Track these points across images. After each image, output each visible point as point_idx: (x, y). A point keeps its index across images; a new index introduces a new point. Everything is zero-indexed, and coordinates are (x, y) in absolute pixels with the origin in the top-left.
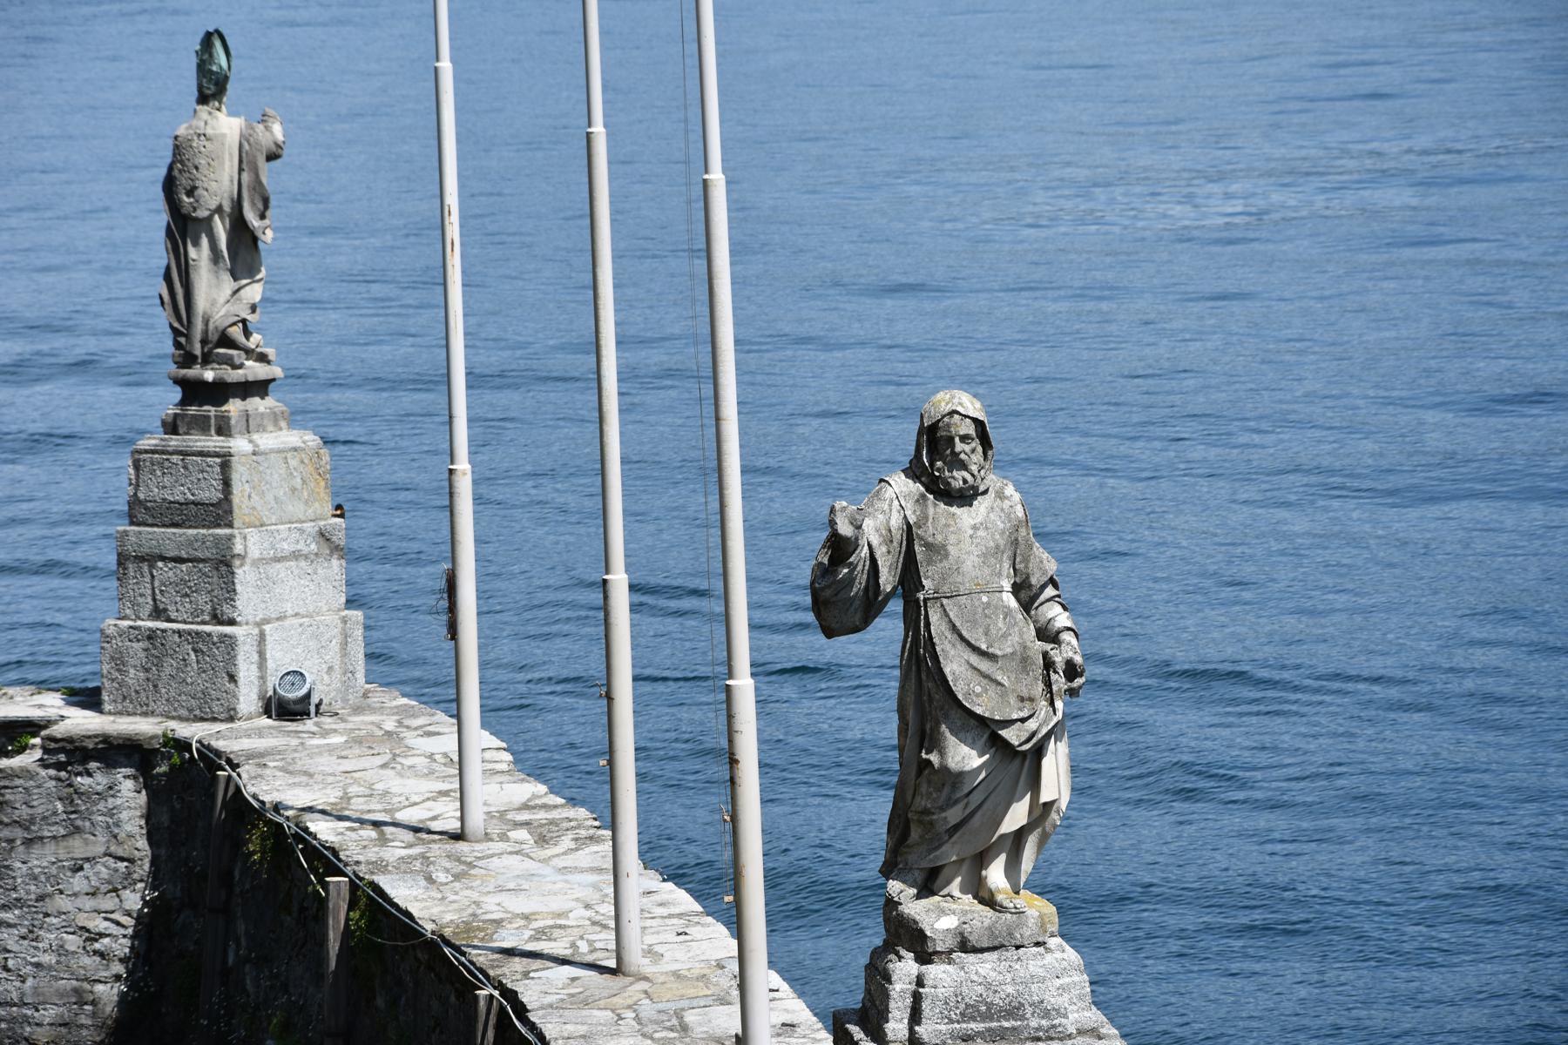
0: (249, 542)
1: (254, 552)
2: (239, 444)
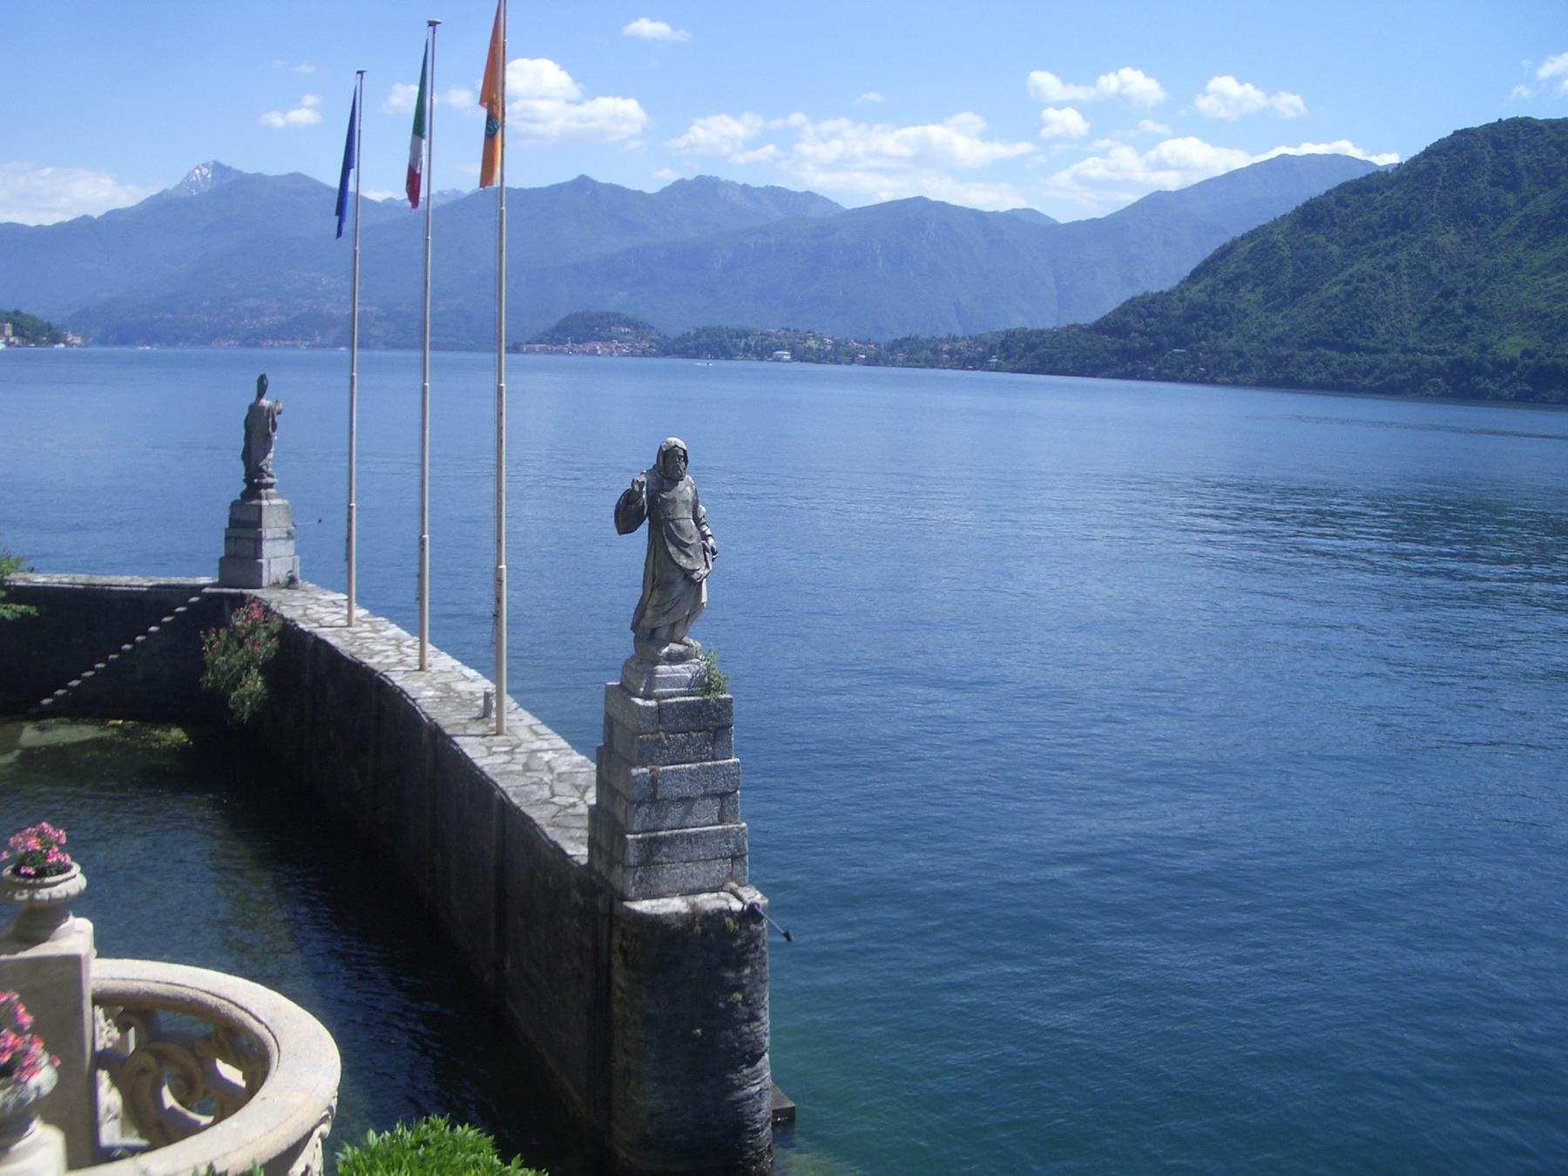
0: (267, 533)
1: (268, 537)
2: (265, 503)
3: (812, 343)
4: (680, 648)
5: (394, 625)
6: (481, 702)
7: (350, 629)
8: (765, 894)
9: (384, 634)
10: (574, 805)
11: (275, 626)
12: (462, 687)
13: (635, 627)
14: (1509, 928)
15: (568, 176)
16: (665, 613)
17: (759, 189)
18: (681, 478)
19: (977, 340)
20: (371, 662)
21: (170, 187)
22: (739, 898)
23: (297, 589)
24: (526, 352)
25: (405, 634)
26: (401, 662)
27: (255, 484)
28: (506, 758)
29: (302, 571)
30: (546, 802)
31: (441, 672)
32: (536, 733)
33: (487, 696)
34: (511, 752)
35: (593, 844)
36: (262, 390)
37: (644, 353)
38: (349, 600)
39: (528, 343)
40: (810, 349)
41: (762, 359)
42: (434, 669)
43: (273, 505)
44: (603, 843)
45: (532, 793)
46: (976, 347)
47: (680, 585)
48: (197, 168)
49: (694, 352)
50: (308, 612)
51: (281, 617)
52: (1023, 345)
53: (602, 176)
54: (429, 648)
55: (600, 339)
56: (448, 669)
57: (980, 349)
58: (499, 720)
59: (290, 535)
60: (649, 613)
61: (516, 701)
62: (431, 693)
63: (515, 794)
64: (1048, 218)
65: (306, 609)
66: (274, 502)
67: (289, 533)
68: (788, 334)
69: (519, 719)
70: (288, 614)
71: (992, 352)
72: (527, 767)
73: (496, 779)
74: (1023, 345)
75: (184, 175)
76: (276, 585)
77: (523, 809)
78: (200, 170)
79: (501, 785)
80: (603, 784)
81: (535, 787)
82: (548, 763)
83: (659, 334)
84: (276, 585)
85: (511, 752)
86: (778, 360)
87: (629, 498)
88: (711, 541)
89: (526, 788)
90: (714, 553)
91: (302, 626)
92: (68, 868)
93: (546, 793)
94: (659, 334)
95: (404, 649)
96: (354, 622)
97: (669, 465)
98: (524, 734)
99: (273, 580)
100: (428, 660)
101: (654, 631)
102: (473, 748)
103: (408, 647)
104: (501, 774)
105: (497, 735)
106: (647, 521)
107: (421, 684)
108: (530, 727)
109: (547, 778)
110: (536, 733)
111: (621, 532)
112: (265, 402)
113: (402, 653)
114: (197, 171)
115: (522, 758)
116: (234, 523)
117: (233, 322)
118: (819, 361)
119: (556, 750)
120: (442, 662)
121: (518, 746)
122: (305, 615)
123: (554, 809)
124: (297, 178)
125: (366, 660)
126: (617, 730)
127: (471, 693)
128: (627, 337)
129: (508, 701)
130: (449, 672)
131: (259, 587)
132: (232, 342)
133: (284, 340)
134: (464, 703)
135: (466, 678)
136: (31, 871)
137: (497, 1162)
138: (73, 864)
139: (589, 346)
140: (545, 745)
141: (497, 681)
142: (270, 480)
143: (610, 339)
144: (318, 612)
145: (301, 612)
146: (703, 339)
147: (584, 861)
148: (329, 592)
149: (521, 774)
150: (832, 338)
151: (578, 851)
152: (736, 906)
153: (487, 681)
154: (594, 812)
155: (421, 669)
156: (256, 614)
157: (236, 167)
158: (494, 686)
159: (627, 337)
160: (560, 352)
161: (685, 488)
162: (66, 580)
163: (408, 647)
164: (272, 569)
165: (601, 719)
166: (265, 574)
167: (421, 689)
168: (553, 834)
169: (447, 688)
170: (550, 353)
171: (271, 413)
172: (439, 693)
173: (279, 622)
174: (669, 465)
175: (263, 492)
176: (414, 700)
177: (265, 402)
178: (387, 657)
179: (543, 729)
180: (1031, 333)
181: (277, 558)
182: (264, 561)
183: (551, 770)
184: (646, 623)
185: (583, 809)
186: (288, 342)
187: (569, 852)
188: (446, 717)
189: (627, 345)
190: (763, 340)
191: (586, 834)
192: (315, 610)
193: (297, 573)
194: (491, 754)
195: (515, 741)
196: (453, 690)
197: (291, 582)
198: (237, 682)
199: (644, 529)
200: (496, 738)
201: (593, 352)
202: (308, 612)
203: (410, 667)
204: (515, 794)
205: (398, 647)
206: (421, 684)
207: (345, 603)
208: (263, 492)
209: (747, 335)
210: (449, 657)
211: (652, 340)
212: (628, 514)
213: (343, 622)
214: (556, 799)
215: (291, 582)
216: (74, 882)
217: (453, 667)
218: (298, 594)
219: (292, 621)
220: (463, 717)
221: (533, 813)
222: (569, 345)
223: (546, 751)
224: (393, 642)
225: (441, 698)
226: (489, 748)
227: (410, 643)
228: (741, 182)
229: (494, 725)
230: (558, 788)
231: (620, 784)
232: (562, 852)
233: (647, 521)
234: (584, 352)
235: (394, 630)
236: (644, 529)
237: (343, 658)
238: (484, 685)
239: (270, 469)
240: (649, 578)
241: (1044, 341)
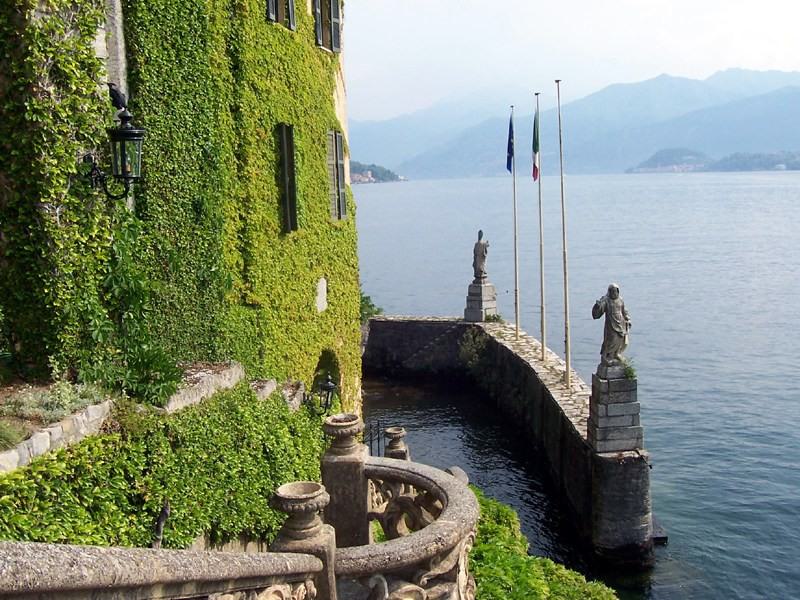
0: (484, 298)
4: (616, 361)
14: (715, 442)
15: (658, 74)
36: (480, 237)
47: (616, 337)
53: (674, 73)
55: (677, 164)
87: (596, 307)
97: (613, 293)
137: (585, 580)
138: (322, 486)
139: (670, 168)
151: (582, 431)
152: (637, 456)
161: (619, 302)
174: (613, 293)
194: (562, 396)
212: (597, 312)
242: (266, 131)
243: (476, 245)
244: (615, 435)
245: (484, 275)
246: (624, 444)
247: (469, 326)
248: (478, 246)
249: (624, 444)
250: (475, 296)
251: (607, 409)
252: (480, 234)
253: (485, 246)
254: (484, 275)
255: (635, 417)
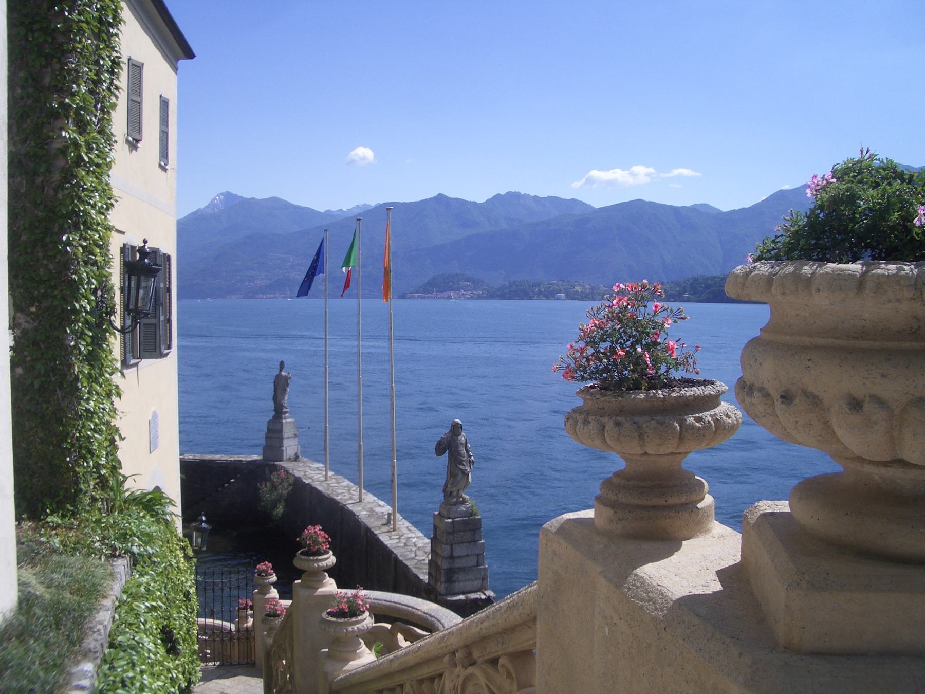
0: (285, 435)
2: (284, 421)
3: (578, 288)
5: (346, 480)
6: (386, 516)
7: (327, 482)
8: (495, 592)
9: (342, 484)
10: (424, 560)
11: (291, 480)
12: (378, 509)
13: (444, 491)
16: (455, 486)
17: (544, 198)
18: (460, 434)
19: (678, 284)
20: (338, 498)
21: (202, 207)
22: (485, 594)
23: (299, 461)
24: (410, 298)
25: (352, 484)
26: (351, 498)
27: (279, 412)
28: (397, 541)
29: (301, 451)
30: (413, 559)
31: (369, 503)
32: (410, 530)
33: (389, 514)
34: (399, 538)
35: (430, 574)
37: (479, 297)
38: (326, 467)
39: (410, 293)
40: (577, 292)
41: (549, 299)
42: (366, 501)
43: (288, 421)
44: (433, 574)
45: (408, 555)
46: (675, 288)
47: (460, 475)
48: (218, 196)
49: (509, 296)
50: (307, 473)
51: (294, 476)
52: (703, 285)
54: (364, 491)
55: (452, 289)
56: (372, 501)
57: (678, 289)
58: (395, 524)
59: (295, 436)
60: (449, 486)
61: (401, 516)
62: (365, 513)
63: (401, 556)
64: (715, 208)
65: (305, 472)
66: (288, 420)
67: (295, 435)
68: (564, 284)
69: (403, 524)
70: (297, 474)
71: (684, 291)
72: (406, 545)
73: (393, 550)
74: (703, 285)
75: (210, 200)
76: (289, 459)
77: (404, 561)
78: (219, 197)
79: (395, 552)
80: (433, 551)
81: (409, 553)
82: (414, 543)
83: (488, 286)
84: (289, 459)
85: (399, 538)
86: (558, 299)
87: (439, 444)
88: (472, 458)
89: (405, 554)
90: (473, 462)
91: (304, 481)
92: (272, 575)
93: (413, 555)
94: (488, 286)
95: (352, 492)
96: (328, 479)
98: (405, 531)
99: (288, 457)
100: (363, 497)
101: (451, 493)
102: (385, 539)
103: (354, 491)
104: (395, 547)
105: (394, 531)
106: (447, 451)
107: (360, 508)
108: (407, 527)
109: (414, 549)
110: (410, 530)
111: (438, 456)
112: (283, 373)
113: (351, 494)
114: (218, 198)
115: (404, 541)
116: (270, 430)
117: (239, 284)
118: (582, 299)
119: (418, 537)
120: (369, 498)
121: (402, 536)
122: (305, 475)
123: (416, 561)
124: (275, 200)
125: (335, 497)
126: (438, 531)
127: (382, 513)
128: (469, 288)
129: (398, 516)
130: (372, 503)
131: (282, 460)
132: (238, 296)
133: (269, 294)
134: (380, 516)
135: (380, 506)
136: (264, 575)
139: (445, 294)
140: (413, 535)
141: (393, 506)
142: (286, 410)
143: (459, 290)
144: (311, 474)
145: (303, 474)
146: (514, 288)
147: (427, 581)
148: (315, 463)
149: (404, 547)
150: (590, 285)
152: (483, 597)
153: (389, 507)
154: (431, 563)
155: (360, 502)
156: (283, 475)
157: (240, 194)
158: (391, 509)
159: (469, 288)
160: (428, 298)
161: (462, 438)
162: (191, 457)
163: (354, 491)
164: (288, 452)
165: (432, 526)
166: (285, 454)
167: (360, 511)
168: (415, 571)
169: (371, 510)
170: (424, 298)
171: (286, 379)
172: (368, 513)
173: (293, 478)
174: (456, 429)
175: (283, 416)
176: (358, 516)
177: (283, 373)
178: (345, 496)
179: (413, 528)
180: (708, 278)
181: (290, 446)
182: (284, 448)
183: (415, 546)
184: (448, 490)
185: (427, 562)
186: (271, 296)
187: (421, 578)
188: (372, 524)
189: (468, 293)
190: (549, 288)
191: (427, 571)
192: (310, 473)
193: (299, 454)
194: (391, 539)
195: (401, 534)
196: (374, 511)
197: (296, 458)
198: (275, 507)
199: (446, 454)
200: (393, 533)
201: (449, 298)
202: (307, 473)
203: (355, 500)
204: (401, 556)
205: (349, 490)
206: (360, 508)
207: (324, 469)
208: (283, 416)
209: (539, 285)
210: (372, 496)
211: (484, 289)
212: (440, 449)
213: (322, 479)
214: (417, 558)
215: (296, 458)
216: (330, 559)
217: (374, 500)
218: (301, 464)
219: (299, 478)
220: (379, 524)
221: (408, 563)
222: (435, 293)
223: (414, 538)
224: (346, 488)
225: (369, 515)
226: (390, 537)
227: (354, 489)
228: (532, 194)
229: (392, 527)
230: (418, 553)
231: (439, 551)
232: (419, 578)
233: (447, 451)
234: (443, 298)
235: (346, 482)
236: (446, 454)
237: (324, 496)
238: (388, 509)
239: (286, 405)
240: (449, 473)
241: (716, 283)
242: (599, 605)
243: (277, 376)
244: (461, 576)
245: (285, 410)
246: (469, 585)
247: (268, 465)
248: (278, 377)
249: (469, 585)
250: (274, 433)
251: (452, 550)
252: (282, 365)
253: (286, 379)
254: (285, 410)
255: (479, 558)
